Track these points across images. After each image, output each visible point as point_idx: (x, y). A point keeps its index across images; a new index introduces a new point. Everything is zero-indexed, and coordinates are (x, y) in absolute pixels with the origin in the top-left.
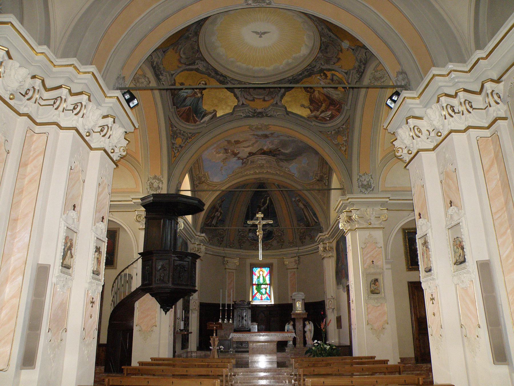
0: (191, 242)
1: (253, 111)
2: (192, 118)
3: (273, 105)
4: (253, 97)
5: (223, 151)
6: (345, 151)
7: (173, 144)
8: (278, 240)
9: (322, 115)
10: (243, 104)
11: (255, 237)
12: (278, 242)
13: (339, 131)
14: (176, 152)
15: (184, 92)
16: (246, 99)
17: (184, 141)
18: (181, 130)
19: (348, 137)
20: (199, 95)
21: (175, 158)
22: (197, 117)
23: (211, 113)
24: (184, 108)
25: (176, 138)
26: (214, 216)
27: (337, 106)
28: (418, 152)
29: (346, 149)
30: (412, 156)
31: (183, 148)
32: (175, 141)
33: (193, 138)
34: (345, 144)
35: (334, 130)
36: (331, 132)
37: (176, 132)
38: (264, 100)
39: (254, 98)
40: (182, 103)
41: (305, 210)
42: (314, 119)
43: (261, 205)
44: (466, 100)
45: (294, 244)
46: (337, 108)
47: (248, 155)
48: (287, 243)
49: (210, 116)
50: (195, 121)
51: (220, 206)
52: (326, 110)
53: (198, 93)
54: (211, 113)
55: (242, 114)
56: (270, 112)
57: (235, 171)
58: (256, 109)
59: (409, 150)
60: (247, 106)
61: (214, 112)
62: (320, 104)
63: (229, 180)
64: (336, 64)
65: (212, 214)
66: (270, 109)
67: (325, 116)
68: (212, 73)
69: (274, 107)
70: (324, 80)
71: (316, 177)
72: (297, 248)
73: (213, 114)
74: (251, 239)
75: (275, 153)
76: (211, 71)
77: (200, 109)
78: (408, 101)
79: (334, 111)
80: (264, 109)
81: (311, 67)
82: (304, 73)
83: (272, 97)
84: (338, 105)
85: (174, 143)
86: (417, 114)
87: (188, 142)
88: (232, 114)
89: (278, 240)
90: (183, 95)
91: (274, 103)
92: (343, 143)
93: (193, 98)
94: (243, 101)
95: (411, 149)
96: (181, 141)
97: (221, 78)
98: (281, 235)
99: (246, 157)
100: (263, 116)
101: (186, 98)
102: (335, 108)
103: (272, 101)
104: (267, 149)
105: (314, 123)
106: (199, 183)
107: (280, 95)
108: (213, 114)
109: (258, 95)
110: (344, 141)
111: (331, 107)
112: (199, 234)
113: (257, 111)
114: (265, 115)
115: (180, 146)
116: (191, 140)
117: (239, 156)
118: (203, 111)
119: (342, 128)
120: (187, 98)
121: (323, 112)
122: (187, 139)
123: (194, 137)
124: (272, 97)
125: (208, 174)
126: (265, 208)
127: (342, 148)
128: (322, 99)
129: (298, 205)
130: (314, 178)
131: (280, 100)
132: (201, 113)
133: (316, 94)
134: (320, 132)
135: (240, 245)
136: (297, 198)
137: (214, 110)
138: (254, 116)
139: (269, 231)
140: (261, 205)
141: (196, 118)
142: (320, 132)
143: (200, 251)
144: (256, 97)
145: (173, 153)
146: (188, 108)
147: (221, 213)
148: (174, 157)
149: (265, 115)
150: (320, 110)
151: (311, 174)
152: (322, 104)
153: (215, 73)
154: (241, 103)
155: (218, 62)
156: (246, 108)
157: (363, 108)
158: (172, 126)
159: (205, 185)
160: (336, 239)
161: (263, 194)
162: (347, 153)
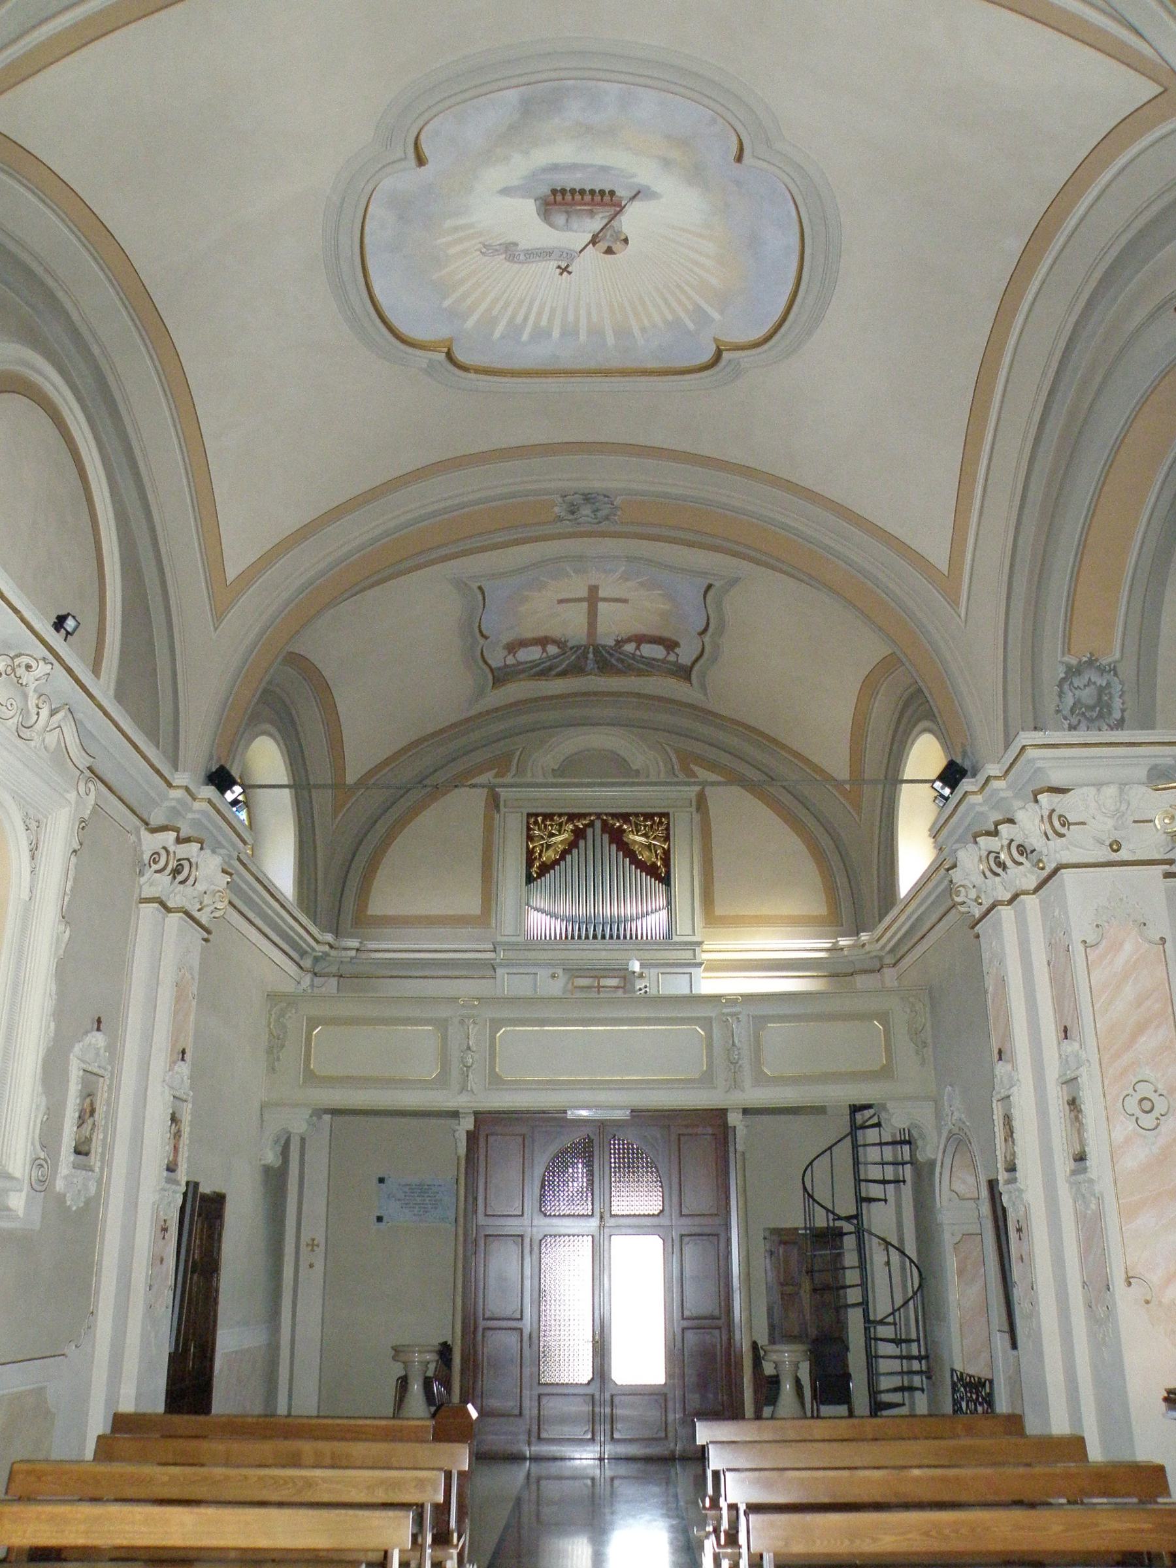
0: (147, 824)
28: (1055, 872)
30: (1045, 873)
44: (990, 852)
59: (1040, 861)
78: (1031, 753)
86: (1055, 783)
95: (1045, 859)
157: (799, 977)
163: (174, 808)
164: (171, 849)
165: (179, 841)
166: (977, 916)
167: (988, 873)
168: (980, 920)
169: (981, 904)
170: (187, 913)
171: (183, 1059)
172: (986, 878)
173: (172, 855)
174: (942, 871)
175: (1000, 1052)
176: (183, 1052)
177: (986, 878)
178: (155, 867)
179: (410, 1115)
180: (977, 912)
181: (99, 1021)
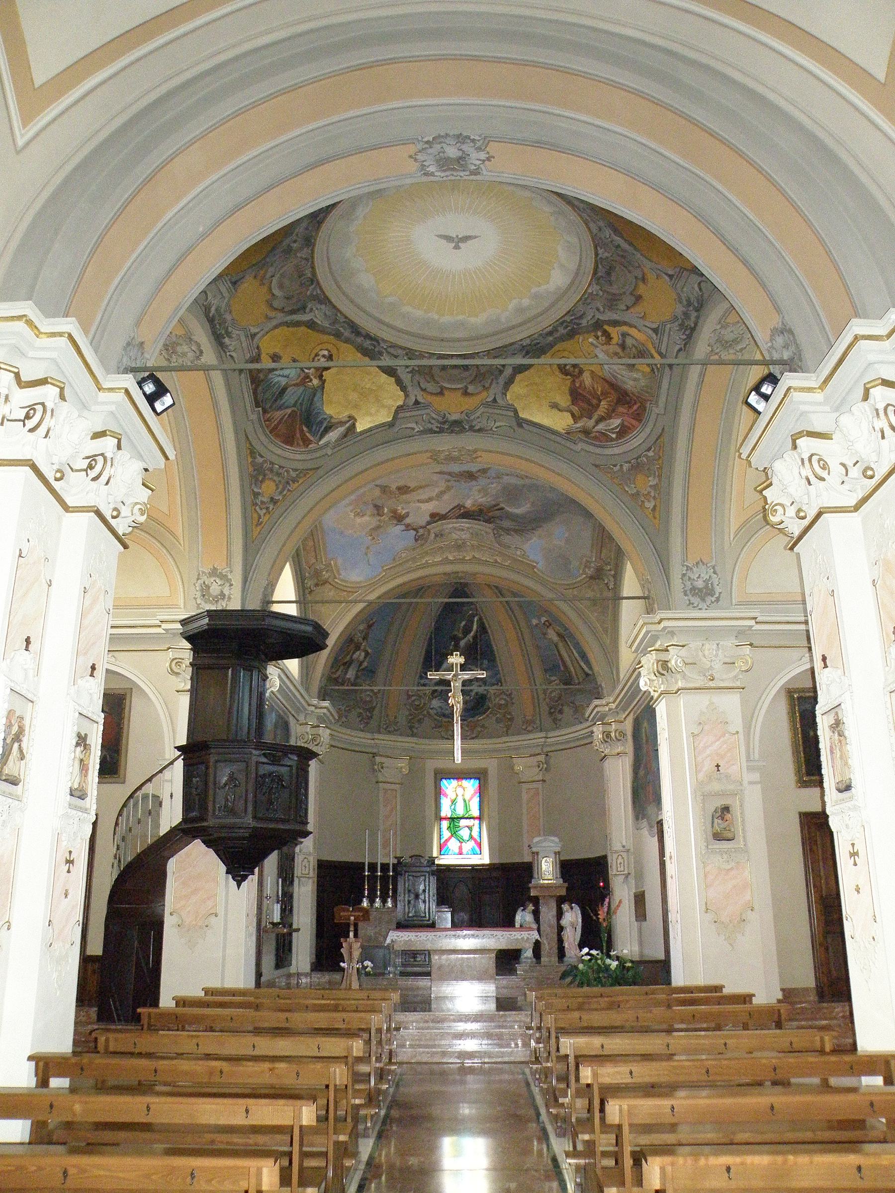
3: (486, 404)
5: (370, 510)
9: (601, 427)
10: (417, 403)
16: (424, 390)
17: (281, 487)
18: (272, 463)
20: (316, 382)
21: (259, 528)
22: (310, 431)
27: (635, 407)
29: (655, 506)
32: (260, 488)
34: (652, 494)
35: (626, 462)
36: (621, 466)
38: (466, 393)
41: (561, 645)
49: (341, 430)
50: (306, 442)
54: (342, 423)
55: (413, 425)
56: (479, 420)
58: (447, 415)
60: (427, 406)
62: (594, 402)
66: (478, 414)
69: (490, 411)
73: (347, 425)
83: (484, 386)
84: (635, 403)
85: (259, 494)
87: (289, 490)
88: (391, 425)
90: (278, 382)
92: (649, 493)
93: (302, 389)
97: (367, 343)
100: (463, 430)
101: (284, 390)
102: (631, 411)
103: (485, 394)
105: (580, 446)
106: (317, 585)
107: (502, 380)
108: (347, 425)
110: (651, 486)
111: (621, 409)
112: (315, 701)
115: (272, 499)
117: (408, 521)
118: (325, 419)
121: (601, 419)
124: (484, 386)
125: (336, 564)
127: (647, 504)
129: (545, 634)
132: (321, 422)
138: (441, 431)
139: (477, 693)
141: (308, 434)
145: (255, 515)
146: (289, 411)
147: (367, 654)
148: (257, 525)
150: (595, 417)
151: (575, 564)
152: (600, 401)
156: (423, 412)
158: (252, 452)
159: (330, 590)
160: (632, 714)
167: (813, 479)
168: (800, 538)
170: (98, 513)
171: (92, 675)
175: (824, 659)
176: (93, 668)
180: (795, 528)
181: (28, 641)
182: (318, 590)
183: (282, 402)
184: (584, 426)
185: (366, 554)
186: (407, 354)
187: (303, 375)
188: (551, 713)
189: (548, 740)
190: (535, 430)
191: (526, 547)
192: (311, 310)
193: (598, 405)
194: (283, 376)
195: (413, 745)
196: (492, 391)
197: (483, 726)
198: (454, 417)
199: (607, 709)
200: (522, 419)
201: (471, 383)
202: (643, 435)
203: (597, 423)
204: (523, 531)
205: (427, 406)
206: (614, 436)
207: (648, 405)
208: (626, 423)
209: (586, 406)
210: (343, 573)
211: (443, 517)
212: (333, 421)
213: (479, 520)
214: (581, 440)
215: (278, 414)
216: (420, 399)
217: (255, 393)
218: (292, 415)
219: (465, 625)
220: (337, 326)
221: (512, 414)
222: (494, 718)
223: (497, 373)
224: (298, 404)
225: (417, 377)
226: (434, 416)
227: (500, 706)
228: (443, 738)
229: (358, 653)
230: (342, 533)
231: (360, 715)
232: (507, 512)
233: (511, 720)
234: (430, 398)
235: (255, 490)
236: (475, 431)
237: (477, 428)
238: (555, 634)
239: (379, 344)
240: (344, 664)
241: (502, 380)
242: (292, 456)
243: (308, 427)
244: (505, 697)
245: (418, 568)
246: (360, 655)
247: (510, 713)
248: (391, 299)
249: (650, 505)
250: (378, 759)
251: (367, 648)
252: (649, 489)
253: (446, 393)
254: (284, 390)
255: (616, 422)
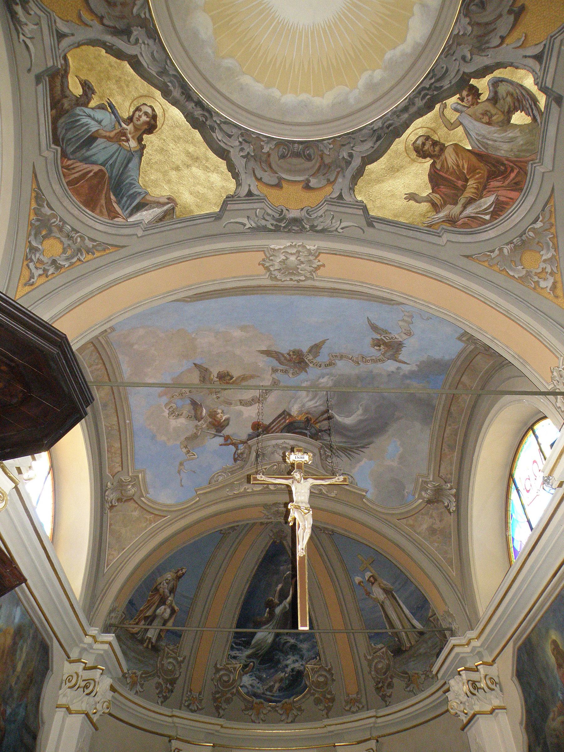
0: (69, 657)
1: (277, 216)
2: (103, 201)
3: (330, 202)
4: (278, 177)
5: (187, 408)
6: (554, 287)
7: (32, 249)
8: (316, 696)
9: (470, 211)
10: (250, 194)
11: (259, 688)
12: (317, 702)
13: (523, 242)
14: (37, 273)
15: (89, 116)
16: (259, 180)
17: (69, 253)
18: (65, 223)
19: (556, 248)
20: (133, 144)
21: (27, 289)
22: (119, 203)
23: (159, 204)
24: (85, 166)
25: (44, 237)
26: (154, 617)
27: (513, 175)
29: (555, 284)
31: (63, 270)
32: (42, 243)
33: (97, 254)
34: (549, 270)
35: (507, 244)
36: (501, 250)
37: (49, 220)
38: (307, 187)
39: (280, 179)
40: (80, 147)
41: (387, 603)
42: (447, 226)
43: (276, 601)
45: (361, 703)
46: (513, 179)
47: (251, 431)
48: (344, 704)
49: (157, 211)
50: (112, 214)
51: (172, 591)
52: (479, 195)
53: (129, 136)
54: (159, 204)
55: (245, 221)
56: (321, 219)
57: (215, 479)
58: (285, 211)
60: (261, 200)
61: (168, 203)
62: (460, 183)
63: (200, 503)
64: (508, 41)
65: (149, 607)
66: (320, 213)
67: (477, 213)
68: (174, 87)
69: (334, 208)
70: (470, 111)
71: (423, 493)
72: (372, 713)
73: (166, 208)
74: (247, 693)
75: (318, 426)
76: (170, 82)
77: (131, 184)
79: (502, 192)
80: (305, 209)
81: (433, 81)
82: (414, 104)
83: (328, 180)
84: (512, 171)
85: (37, 250)
87: (79, 260)
88: (217, 217)
89: (316, 696)
90: (83, 125)
91: (335, 195)
92: (544, 269)
93: (115, 147)
94: (249, 186)
96: (61, 251)
97: (198, 112)
98: (326, 683)
99: (244, 437)
100: (302, 230)
101: (92, 139)
102: (507, 183)
103: (329, 189)
104: (300, 412)
105: (446, 237)
106: (119, 500)
107: (349, 173)
108: (166, 208)
109: (290, 171)
110: (545, 261)
111: (494, 184)
112: (94, 631)
113: (287, 217)
114: (308, 227)
115: (54, 262)
116: (90, 257)
117: (227, 431)
118: (139, 194)
119: (533, 230)
120: (97, 138)
121: (470, 201)
122: (79, 250)
123: (102, 253)
124: (328, 180)
125: (144, 478)
126: (285, 607)
127: (543, 284)
128: (466, 166)
129: (368, 594)
130: (416, 497)
131: (350, 189)
132: (133, 197)
133: (450, 157)
134: (467, 257)
135: (217, 708)
136: (368, 574)
137: (169, 199)
138: (277, 229)
139: (293, 670)
140: (276, 601)
141: (115, 205)
142: (467, 257)
143: (91, 688)
144: (284, 176)
145: (26, 273)
146: (96, 168)
147: (173, 611)
148: (25, 285)
149: (308, 227)
150: (462, 201)
151: (409, 488)
152: (467, 180)
153: (183, 93)
154: (244, 191)
155: (190, 58)
156: (255, 206)
158: (39, 197)
159: (135, 509)
160: (511, 643)
161: (282, 568)
162: (559, 292)
163: (102, 655)
164: (80, 674)
165: (85, 669)
166: (465, 721)
169: (466, 714)
172: (468, 697)
173: (80, 677)
174: (441, 692)
177: (468, 697)
178: (68, 685)
179: (421, 55)
182: (119, 506)
183: (89, 153)
184: (447, 216)
185: (179, 472)
186: (242, 135)
187: (118, 129)
188: (378, 689)
189: (379, 720)
190: (388, 228)
191: (355, 472)
192: (137, 40)
193: (465, 187)
194: (94, 119)
195: (218, 728)
196: (337, 187)
197: (300, 709)
198: (294, 214)
199: (467, 649)
200: (373, 217)
201: (313, 175)
202: (527, 205)
203: (465, 207)
204: (351, 449)
205: (261, 200)
206: (487, 217)
207: (529, 168)
208: (502, 199)
209: (450, 192)
210: (151, 491)
211: (267, 429)
212: (148, 198)
213: (305, 435)
214: (446, 231)
215: (83, 167)
216: (255, 191)
217: (55, 121)
218: (100, 174)
219: (282, 589)
220: (166, 79)
221: (361, 212)
222: (312, 698)
223: (343, 164)
224: (108, 165)
225: (252, 164)
226: (270, 211)
227: (318, 685)
228: (253, 722)
229: (163, 607)
230: (153, 437)
231: (158, 685)
232: (337, 423)
233: (332, 700)
234: (266, 191)
235: (34, 244)
236: (317, 232)
237: (319, 228)
238: (381, 591)
239: (211, 116)
240: (146, 618)
241: (349, 173)
242: (91, 223)
243: (116, 196)
244: (324, 673)
245: (236, 497)
246: (164, 611)
247: (330, 693)
248: (228, 62)
249: (546, 284)
250: (148, 522)
251: (174, 604)
252: (543, 265)
253: (284, 185)
254: (92, 139)
255: (488, 201)
